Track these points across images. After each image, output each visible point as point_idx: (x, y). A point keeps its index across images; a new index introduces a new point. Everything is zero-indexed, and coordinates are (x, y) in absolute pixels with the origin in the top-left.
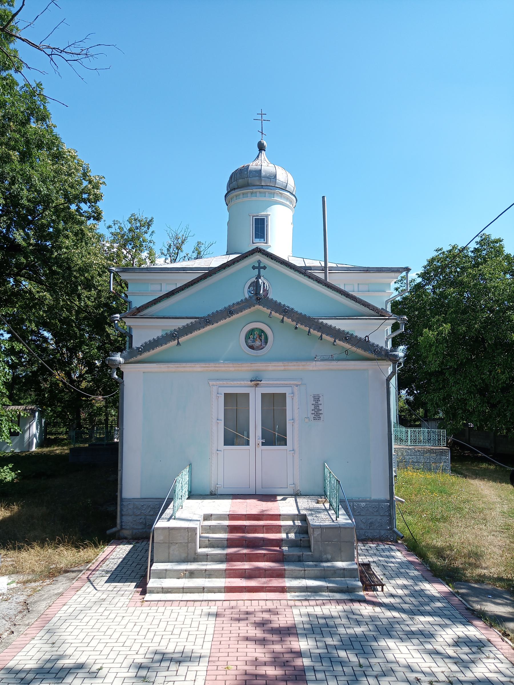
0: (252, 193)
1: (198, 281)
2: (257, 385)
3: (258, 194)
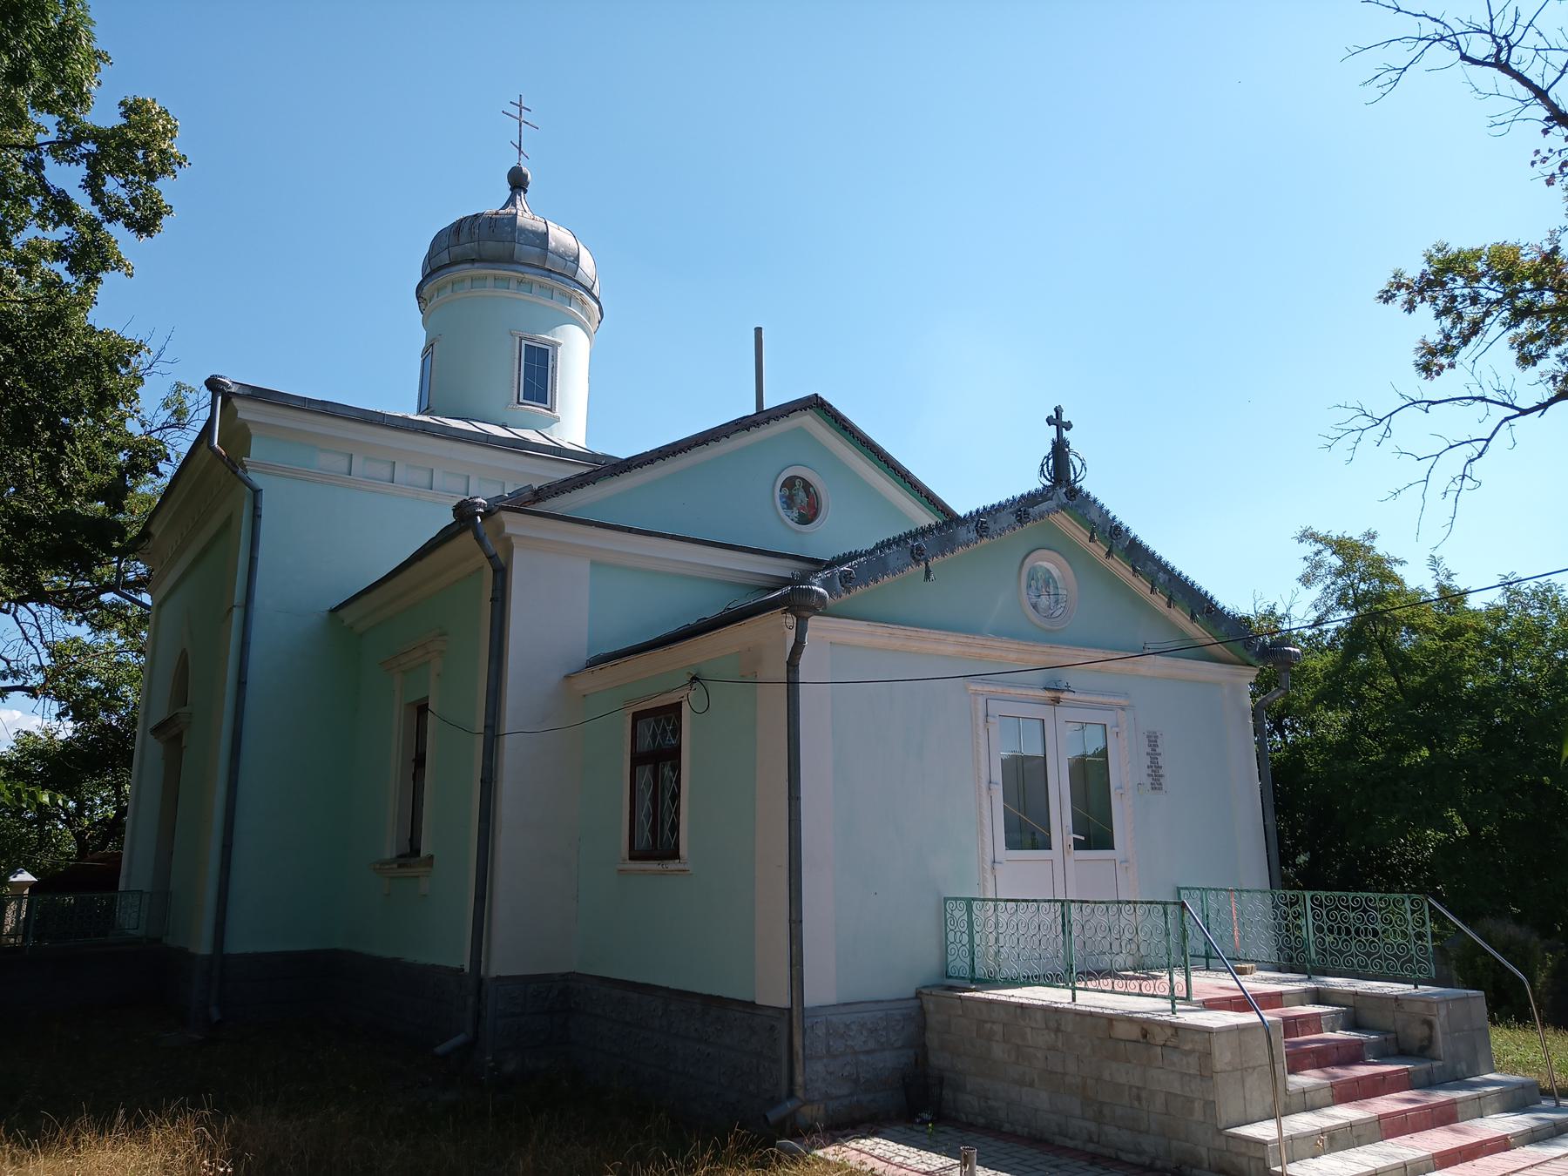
0: (520, 282)
1: (652, 462)
2: (1057, 701)
3: (513, 284)
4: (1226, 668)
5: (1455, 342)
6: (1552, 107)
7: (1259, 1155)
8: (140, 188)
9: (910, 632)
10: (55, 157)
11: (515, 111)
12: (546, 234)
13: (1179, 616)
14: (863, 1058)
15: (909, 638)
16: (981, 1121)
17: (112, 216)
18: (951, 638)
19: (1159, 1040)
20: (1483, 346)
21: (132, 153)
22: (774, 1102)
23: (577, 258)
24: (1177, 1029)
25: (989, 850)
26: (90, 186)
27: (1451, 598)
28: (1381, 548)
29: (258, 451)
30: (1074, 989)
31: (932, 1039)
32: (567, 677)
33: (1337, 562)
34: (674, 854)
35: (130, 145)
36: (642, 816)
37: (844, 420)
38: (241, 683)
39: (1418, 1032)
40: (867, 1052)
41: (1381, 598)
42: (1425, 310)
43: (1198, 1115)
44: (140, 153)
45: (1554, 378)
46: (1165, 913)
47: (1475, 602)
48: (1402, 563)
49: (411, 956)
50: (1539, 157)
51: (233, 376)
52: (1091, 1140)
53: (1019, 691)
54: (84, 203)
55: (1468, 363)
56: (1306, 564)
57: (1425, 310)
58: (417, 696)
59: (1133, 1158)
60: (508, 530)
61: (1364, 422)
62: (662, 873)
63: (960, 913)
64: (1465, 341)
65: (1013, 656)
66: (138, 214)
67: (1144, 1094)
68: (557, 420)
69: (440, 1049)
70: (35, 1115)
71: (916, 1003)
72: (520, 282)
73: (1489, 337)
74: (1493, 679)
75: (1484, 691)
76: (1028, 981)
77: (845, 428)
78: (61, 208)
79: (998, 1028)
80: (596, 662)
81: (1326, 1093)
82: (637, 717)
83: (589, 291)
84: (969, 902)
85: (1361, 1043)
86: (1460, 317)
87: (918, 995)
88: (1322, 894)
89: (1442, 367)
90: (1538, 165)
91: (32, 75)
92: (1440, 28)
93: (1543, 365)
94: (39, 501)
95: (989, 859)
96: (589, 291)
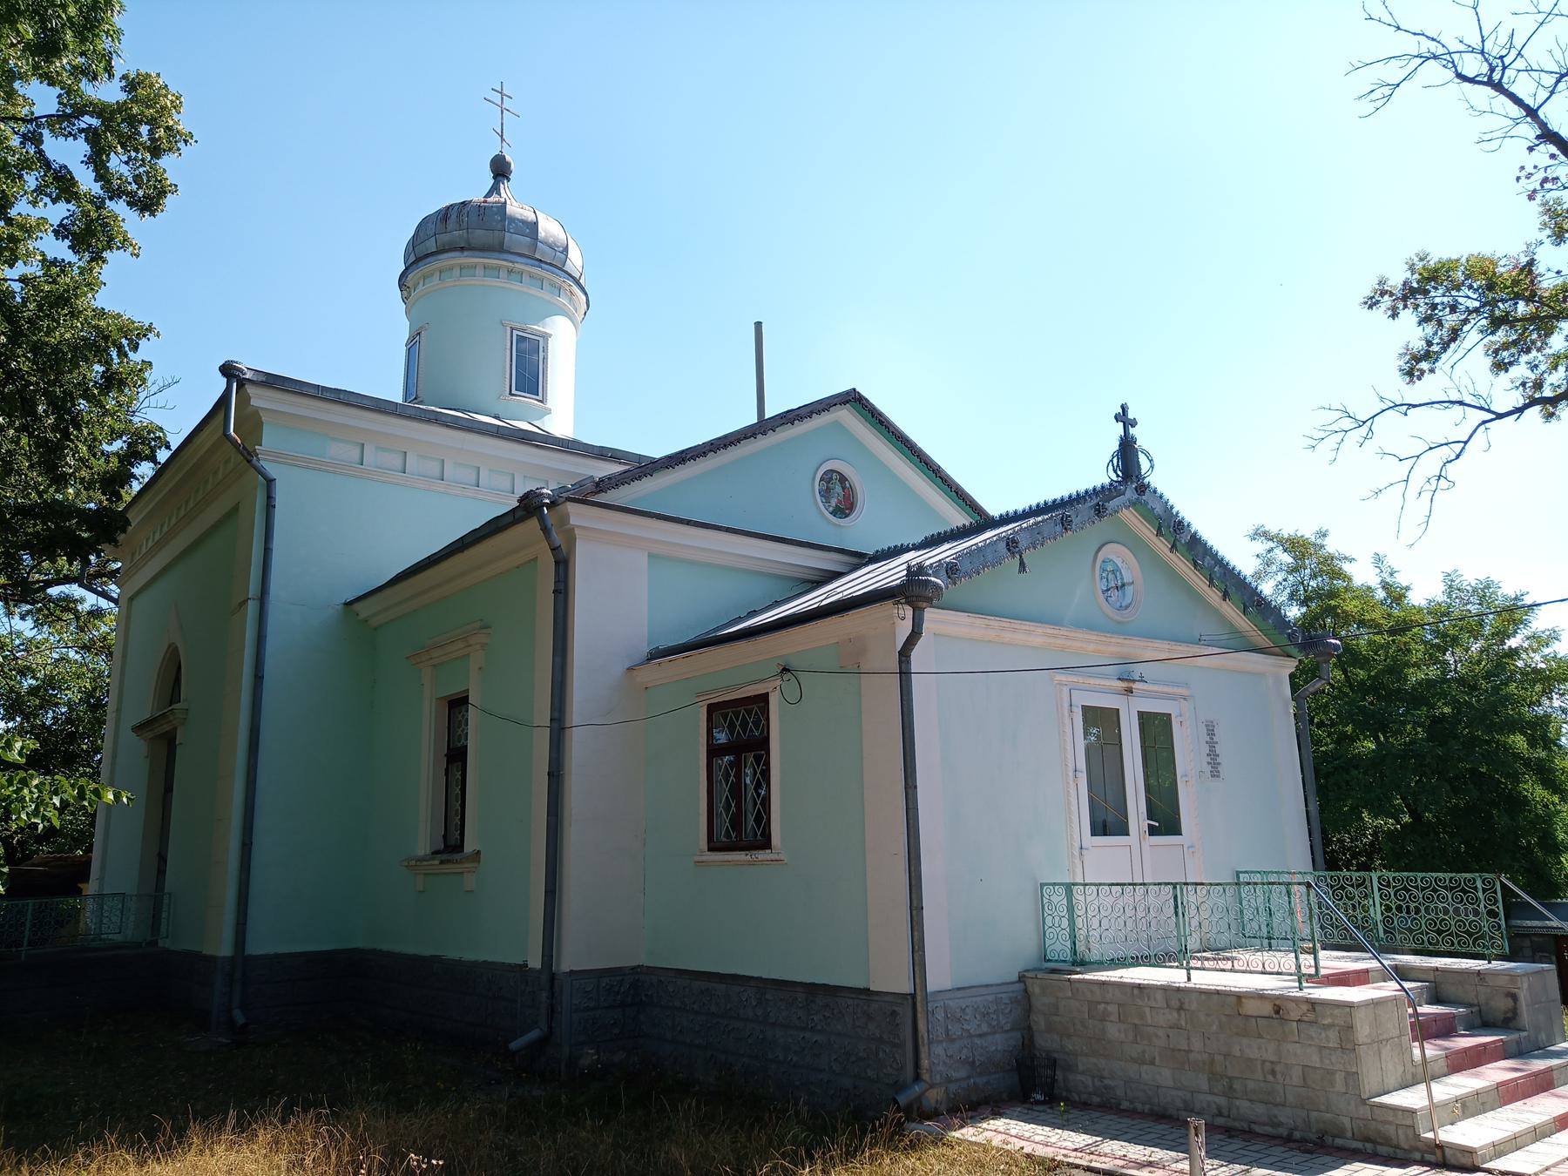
0: (510, 271)
1: (705, 454)
2: (1130, 691)
3: (503, 274)
4: (1271, 660)
5: (1435, 348)
6: (1543, 125)
7: (1408, 1123)
8: (143, 165)
9: (1005, 623)
10: (52, 131)
11: (497, 98)
12: (536, 224)
13: (1230, 611)
14: (978, 1041)
15: (1003, 629)
16: (1096, 1100)
17: (115, 194)
18: (1040, 629)
19: (1294, 1015)
20: (1461, 352)
21: (136, 128)
22: (900, 1087)
23: (566, 249)
24: (1313, 1004)
25: (1076, 836)
26: (94, 162)
27: (1396, 595)
28: (1332, 546)
29: (271, 440)
30: (1188, 969)
31: (1039, 1022)
32: (630, 669)
33: (1287, 559)
34: (766, 845)
35: (133, 121)
36: (720, 808)
37: (881, 414)
38: (258, 678)
39: (1502, 1004)
40: (980, 1036)
41: (1333, 594)
42: (1408, 317)
43: (1339, 1086)
44: (144, 129)
45: (1524, 384)
46: (1289, 893)
47: (1417, 598)
48: (1352, 560)
49: (452, 954)
50: (1523, 174)
51: (249, 362)
52: (1220, 1114)
53: (1098, 681)
54: (86, 180)
55: (1447, 368)
56: (1259, 561)
57: (1408, 317)
58: (453, 690)
59: (1269, 1130)
60: (573, 521)
61: (1347, 424)
62: (751, 863)
63: (1059, 898)
64: (1445, 346)
65: (1092, 647)
66: (141, 193)
67: (1278, 1068)
68: (549, 411)
69: (514, 1045)
70: (47, 1124)
71: (1020, 986)
72: (510, 271)
73: (1467, 344)
74: (1433, 672)
75: (1429, 683)
76: (1136, 961)
77: (881, 423)
78: (63, 185)
79: (1113, 1009)
80: (657, 654)
81: (1442, 1063)
82: (712, 709)
83: (577, 282)
84: (1069, 887)
85: (1453, 1016)
86: (1440, 324)
87: (1022, 978)
88: (1391, 875)
89: (1422, 372)
90: (1523, 180)
91: (66, 46)
92: (1433, 46)
93: (1513, 370)
94: (27, 485)
95: (1077, 845)
96: (577, 282)
